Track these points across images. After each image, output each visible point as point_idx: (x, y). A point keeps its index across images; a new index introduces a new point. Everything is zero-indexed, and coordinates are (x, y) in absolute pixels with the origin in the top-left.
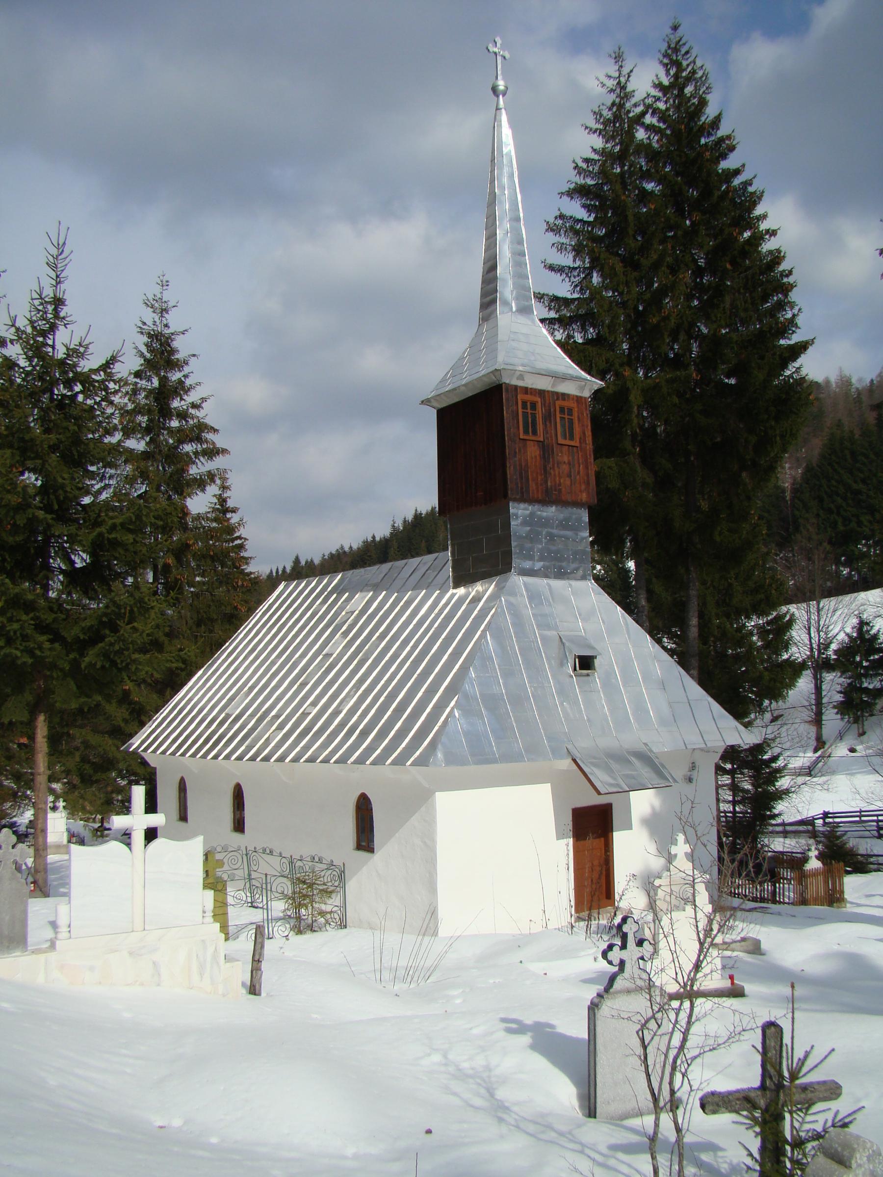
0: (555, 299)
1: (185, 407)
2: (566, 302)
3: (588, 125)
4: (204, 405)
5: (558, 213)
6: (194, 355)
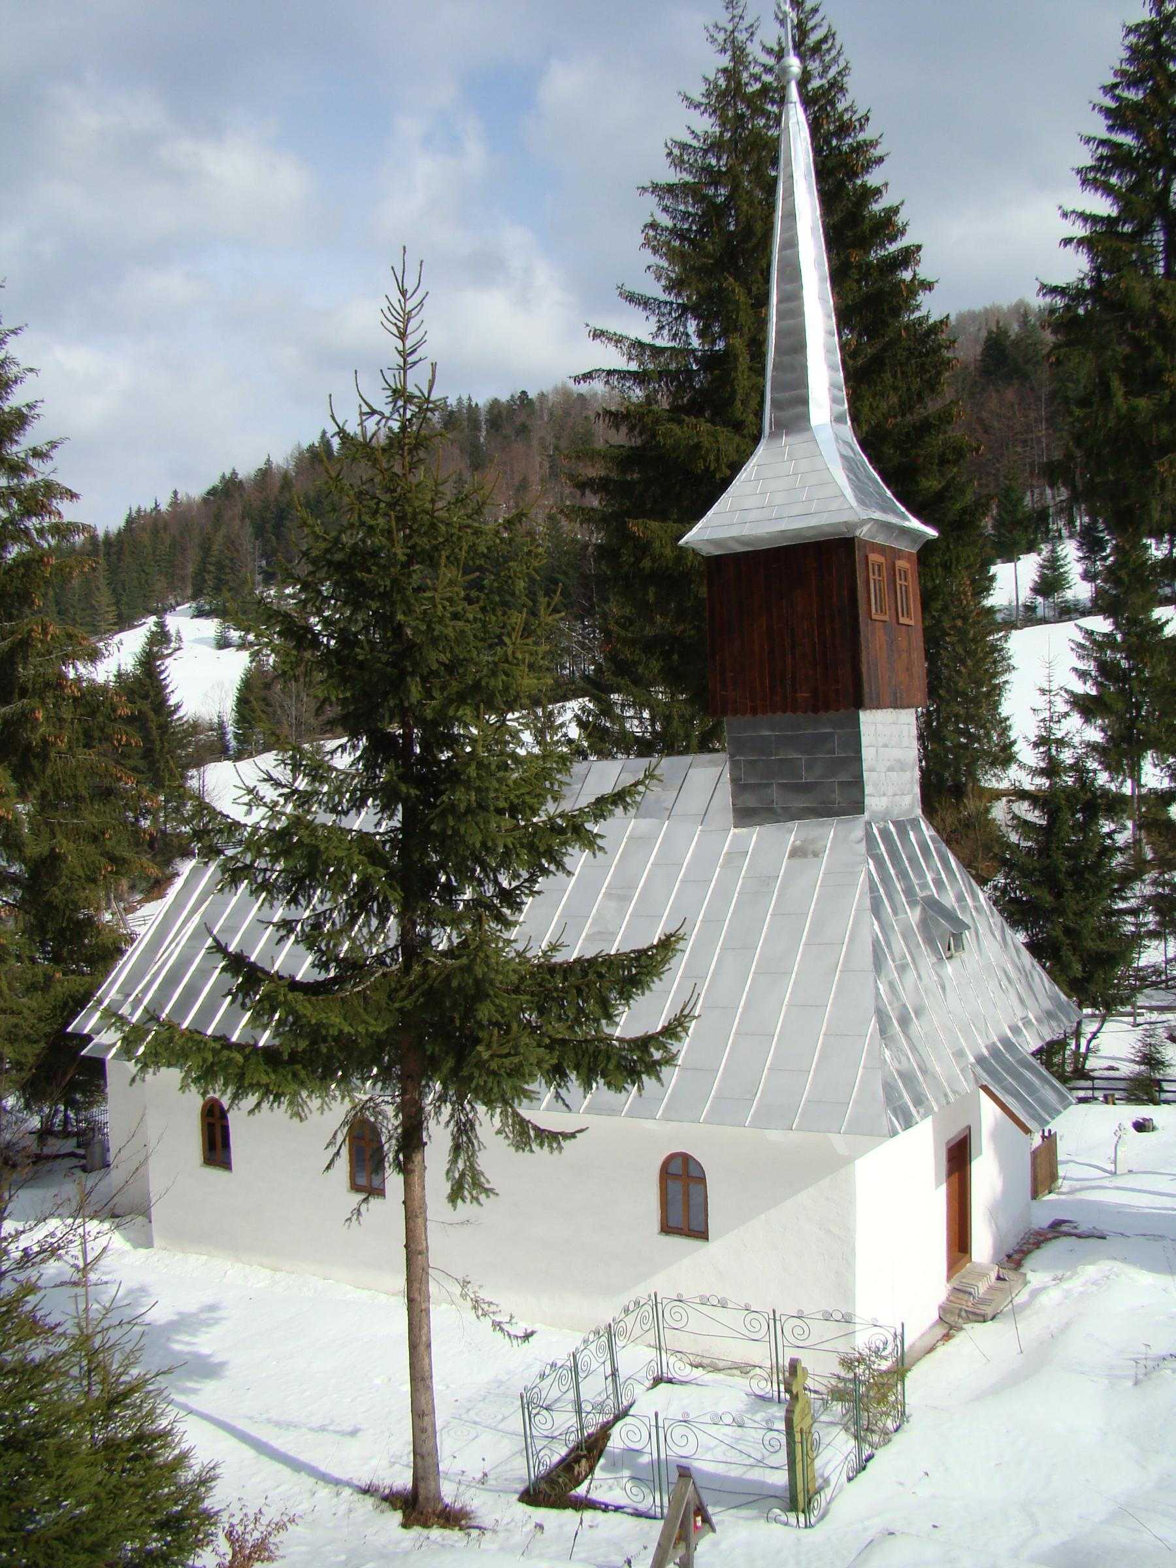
0: (639, 345)
1: (22, 455)
2: (657, 351)
3: (688, 95)
4: (53, 453)
5: (649, 220)
6: (31, 370)
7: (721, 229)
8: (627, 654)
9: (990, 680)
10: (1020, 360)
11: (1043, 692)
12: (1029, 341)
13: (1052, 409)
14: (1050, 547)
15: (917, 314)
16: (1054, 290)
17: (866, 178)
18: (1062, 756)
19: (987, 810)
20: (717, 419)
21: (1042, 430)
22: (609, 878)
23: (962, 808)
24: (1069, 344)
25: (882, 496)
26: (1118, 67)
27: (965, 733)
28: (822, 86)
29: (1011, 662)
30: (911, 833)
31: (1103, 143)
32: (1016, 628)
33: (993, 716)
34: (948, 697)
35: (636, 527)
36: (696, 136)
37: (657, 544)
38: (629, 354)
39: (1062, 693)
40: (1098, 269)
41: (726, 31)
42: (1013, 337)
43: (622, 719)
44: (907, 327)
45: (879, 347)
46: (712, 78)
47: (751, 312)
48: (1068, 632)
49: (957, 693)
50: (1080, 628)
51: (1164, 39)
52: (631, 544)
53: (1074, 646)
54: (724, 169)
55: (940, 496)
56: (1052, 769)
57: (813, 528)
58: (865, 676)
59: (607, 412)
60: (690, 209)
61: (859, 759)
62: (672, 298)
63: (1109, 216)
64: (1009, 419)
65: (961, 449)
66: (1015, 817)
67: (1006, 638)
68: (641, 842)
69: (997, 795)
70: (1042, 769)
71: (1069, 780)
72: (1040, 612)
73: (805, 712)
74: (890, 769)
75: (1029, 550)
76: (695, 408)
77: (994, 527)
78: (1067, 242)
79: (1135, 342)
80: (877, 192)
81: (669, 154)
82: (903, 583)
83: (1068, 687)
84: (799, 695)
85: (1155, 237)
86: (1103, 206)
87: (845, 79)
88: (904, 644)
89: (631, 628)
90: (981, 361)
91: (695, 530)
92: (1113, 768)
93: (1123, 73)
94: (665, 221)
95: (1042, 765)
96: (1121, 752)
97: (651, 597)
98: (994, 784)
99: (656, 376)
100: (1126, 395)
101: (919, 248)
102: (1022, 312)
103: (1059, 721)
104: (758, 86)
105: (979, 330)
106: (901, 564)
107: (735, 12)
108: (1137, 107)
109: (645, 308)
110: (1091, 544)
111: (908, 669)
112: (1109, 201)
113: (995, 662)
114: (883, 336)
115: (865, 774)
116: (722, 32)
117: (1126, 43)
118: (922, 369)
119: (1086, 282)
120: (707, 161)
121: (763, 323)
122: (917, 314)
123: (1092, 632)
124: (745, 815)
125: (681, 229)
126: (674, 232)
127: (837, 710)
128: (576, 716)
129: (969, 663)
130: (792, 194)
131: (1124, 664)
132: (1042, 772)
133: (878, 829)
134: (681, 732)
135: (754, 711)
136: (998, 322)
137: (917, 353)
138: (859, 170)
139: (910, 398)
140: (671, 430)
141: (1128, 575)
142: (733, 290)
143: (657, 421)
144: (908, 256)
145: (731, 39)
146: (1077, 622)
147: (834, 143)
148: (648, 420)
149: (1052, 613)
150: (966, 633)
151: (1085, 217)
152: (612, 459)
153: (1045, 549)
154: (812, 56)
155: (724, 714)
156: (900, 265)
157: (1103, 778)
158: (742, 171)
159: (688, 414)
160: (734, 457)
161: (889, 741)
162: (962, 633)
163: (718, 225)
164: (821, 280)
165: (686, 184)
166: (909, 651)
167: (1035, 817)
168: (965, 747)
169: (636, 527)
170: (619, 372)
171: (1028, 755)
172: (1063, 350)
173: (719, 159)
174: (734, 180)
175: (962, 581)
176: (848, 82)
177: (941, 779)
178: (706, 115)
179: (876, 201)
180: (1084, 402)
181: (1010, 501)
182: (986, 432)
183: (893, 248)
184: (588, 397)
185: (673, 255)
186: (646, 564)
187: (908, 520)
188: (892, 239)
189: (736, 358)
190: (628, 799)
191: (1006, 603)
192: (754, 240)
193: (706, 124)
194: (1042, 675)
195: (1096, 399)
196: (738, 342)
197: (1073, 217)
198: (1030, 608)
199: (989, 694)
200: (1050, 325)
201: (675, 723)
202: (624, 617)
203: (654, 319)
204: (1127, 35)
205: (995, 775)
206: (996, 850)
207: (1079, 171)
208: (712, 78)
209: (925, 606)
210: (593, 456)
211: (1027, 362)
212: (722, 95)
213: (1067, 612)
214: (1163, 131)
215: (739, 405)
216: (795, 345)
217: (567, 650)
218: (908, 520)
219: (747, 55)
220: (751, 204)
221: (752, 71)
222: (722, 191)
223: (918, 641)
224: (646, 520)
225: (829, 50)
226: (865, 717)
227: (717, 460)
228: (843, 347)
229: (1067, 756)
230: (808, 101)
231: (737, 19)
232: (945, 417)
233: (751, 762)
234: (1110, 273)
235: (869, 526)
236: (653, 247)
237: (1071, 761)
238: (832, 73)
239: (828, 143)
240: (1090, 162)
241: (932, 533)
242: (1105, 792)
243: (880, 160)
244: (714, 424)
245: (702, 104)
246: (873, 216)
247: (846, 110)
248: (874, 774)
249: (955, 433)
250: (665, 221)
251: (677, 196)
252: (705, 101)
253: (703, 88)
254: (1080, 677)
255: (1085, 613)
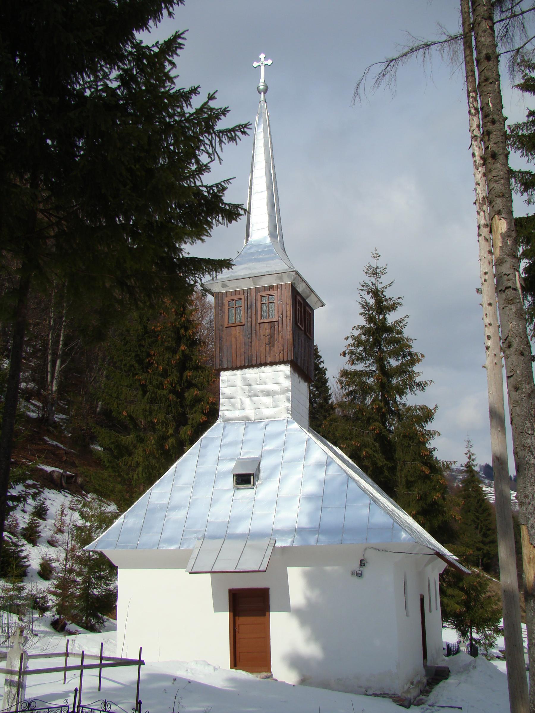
5: (527, 113)
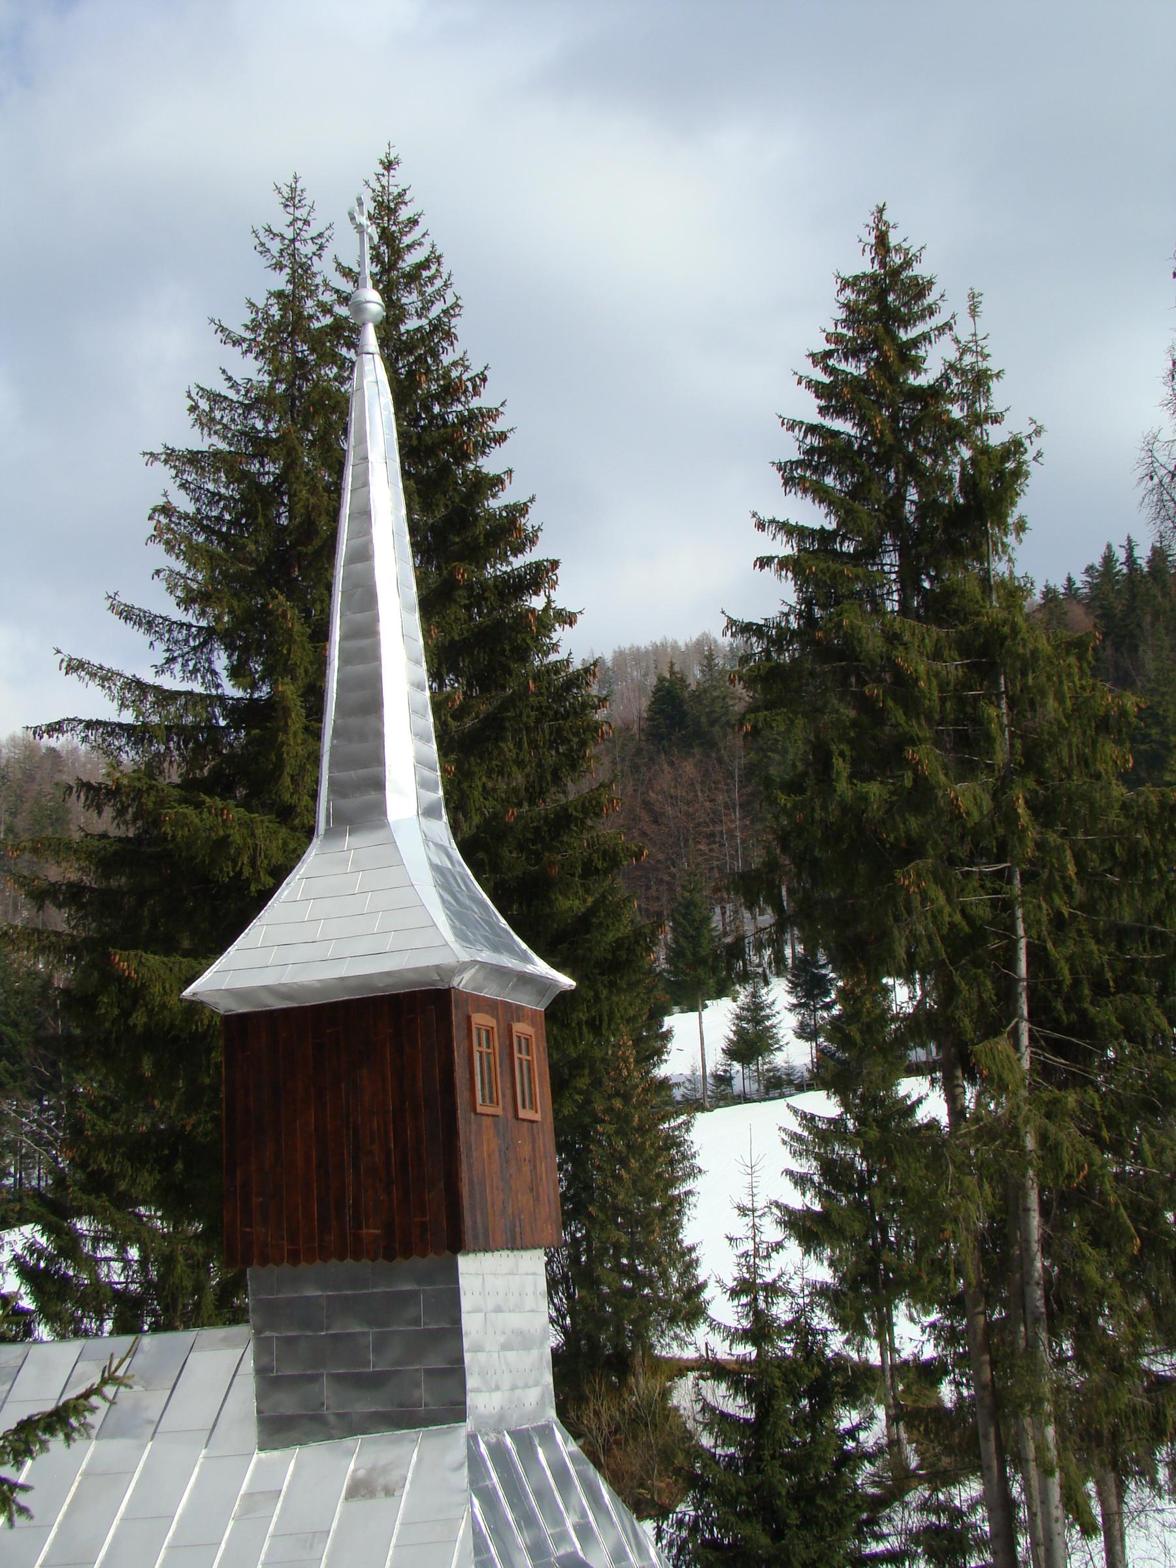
2: (166, 697)
5: (161, 501)
7: (269, 523)
8: (102, 1161)
9: (665, 1190)
10: (703, 719)
11: (743, 1211)
12: (715, 694)
13: (749, 790)
14: (750, 989)
15: (553, 657)
16: (747, 629)
17: (482, 461)
18: (774, 1310)
19: (666, 1394)
20: (254, 802)
21: (735, 821)
22: (46, 1548)
23: (626, 1395)
24: (769, 706)
25: (493, 926)
26: (832, 330)
27: (631, 1273)
28: (421, 328)
29: (698, 1162)
30: (540, 1450)
31: (812, 429)
32: (702, 1108)
33: (671, 1244)
34: (602, 1217)
35: (124, 962)
36: (234, 386)
37: (157, 989)
38: (123, 699)
39: (775, 1210)
40: (807, 601)
41: (283, 238)
42: (693, 687)
43: (93, 1263)
44: (537, 677)
45: (496, 703)
46: (261, 304)
47: (309, 646)
48: (772, 1120)
49: (617, 1210)
50: (795, 1111)
51: (891, 298)
52: (114, 988)
53: (786, 1138)
54: (274, 436)
55: (584, 923)
56: (760, 1330)
57: (388, 974)
58: (466, 1202)
59: (87, 786)
60: (223, 491)
61: (455, 1330)
62: (189, 617)
63: (822, 528)
64: (688, 803)
65: (615, 853)
66: (707, 1408)
67: (687, 1125)
68: (106, 1478)
69: (681, 1369)
70: (745, 1331)
71: (787, 1347)
72: (738, 1085)
73: (374, 1259)
74: (506, 1347)
75: (720, 993)
76: (220, 784)
77: (668, 960)
78: (763, 562)
79: (864, 704)
80: (497, 482)
81: (193, 409)
82: (524, 1056)
83: (781, 1201)
84: (364, 1231)
85: (887, 560)
86: (813, 515)
87: (454, 321)
88: (525, 1150)
89: (114, 1116)
90: (649, 719)
91: (208, 974)
92: (852, 1324)
93: (838, 339)
94: (184, 503)
95: (746, 1324)
96: (862, 1296)
97: (147, 1067)
98: (676, 1351)
99: (162, 733)
100: (851, 777)
101: (555, 564)
102: (705, 652)
103: (768, 1256)
104: (328, 320)
105: (646, 675)
106: (520, 1028)
107: (298, 214)
108: (855, 383)
109: (149, 630)
110: (809, 987)
111: (533, 1188)
112: (823, 510)
113: (672, 1162)
114: (503, 688)
115: (467, 1357)
116: (278, 239)
117: (842, 299)
118: (558, 737)
119: (792, 618)
120: (250, 422)
121: (322, 663)
122: (553, 657)
123: (813, 1117)
124: (278, 1429)
125: (208, 518)
126: (197, 521)
127: (423, 1255)
128: (16, 1258)
129: (634, 1164)
130: (366, 484)
131: (861, 1165)
132: (745, 1336)
133: (488, 1444)
134: (188, 1284)
135: (294, 1258)
136: (672, 665)
137: (551, 713)
138: (471, 451)
139: (542, 777)
140: (185, 816)
141: (862, 1033)
142: (284, 615)
143: (161, 803)
144: (540, 576)
145: (290, 248)
146: (789, 1100)
147: (436, 409)
148: (149, 802)
149: (755, 1086)
150: (627, 1119)
151: (789, 530)
152: (89, 855)
153: (744, 994)
154: (407, 285)
155: (248, 1262)
156: (528, 588)
157: (836, 1342)
158: (301, 441)
159: (210, 793)
160: (278, 859)
161: (506, 1302)
162: (622, 1119)
163: (265, 515)
164: (406, 608)
165: (217, 454)
166: (533, 1161)
167: (736, 1406)
168: (630, 1294)
169: (124, 962)
170: (104, 724)
171: (725, 1310)
172: (761, 715)
173: (267, 421)
174: (289, 454)
175: (622, 1041)
176: (458, 325)
177: (594, 1346)
178: (251, 356)
179: (494, 496)
180: (794, 787)
181: (691, 924)
182: (655, 821)
183: (519, 562)
184: (64, 754)
185: (192, 555)
186: (139, 1019)
187: (532, 962)
188: (518, 550)
189: (287, 711)
190: (74, 1421)
191: (687, 1072)
192: (317, 543)
193: (250, 369)
194: (741, 1181)
195: (810, 782)
196: (290, 690)
197: (772, 528)
198: (723, 1080)
199: (663, 1212)
200: (740, 679)
201: (180, 1268)
202: (104, 1098)
203: (160, 646)
204: (842, 289)
205: (676, 1337)
206: (680, 1459)
207: (781, 467)
208: (261, 305)
209: (560, 1085)
210: (61, 849)
211: (712, 724)
212: (275, 329)
213: (776, 1085)
214: (894, 418)
215: (287, 781)
216: (367, 702)
217: (12, 1147)
218: (532, 962)
219: (314, 275)
220: (313, 491)
221: (321, 298)
222: (270, 467)
223: (547, 1140)
224: (140, 952)
225: (431, 279)
226: (469, 1266)
227: (253, 863)
228: (439, 706)
229: (782, 1310)
230: (394, 347)
231: (300, 224)
232: (592, 807)
233: (290, 1340)
234: (823, 607)
235: (473, 971)
236: (167, 543)
237: (788, 1317)
238: (436, 310)
239: (428, 409)
240: (796, 456)
241: (566, 981)
242: (840, 1362)
243: (502, 437)
244: (250, 810)
245: (244, 340)
246: (491, 516)
247: (455, 364)
248: (481, 1356)
249: (607, 829)
250: (184, 503)
251: (203, 468)
252: (248, 335)
253: (248, 317)
254: (796, 1184)
255: (802, 1087)
